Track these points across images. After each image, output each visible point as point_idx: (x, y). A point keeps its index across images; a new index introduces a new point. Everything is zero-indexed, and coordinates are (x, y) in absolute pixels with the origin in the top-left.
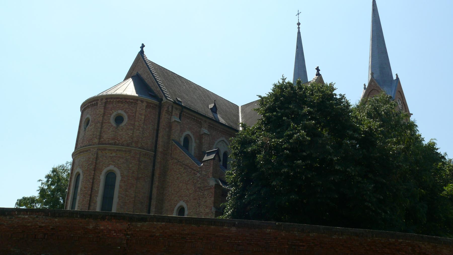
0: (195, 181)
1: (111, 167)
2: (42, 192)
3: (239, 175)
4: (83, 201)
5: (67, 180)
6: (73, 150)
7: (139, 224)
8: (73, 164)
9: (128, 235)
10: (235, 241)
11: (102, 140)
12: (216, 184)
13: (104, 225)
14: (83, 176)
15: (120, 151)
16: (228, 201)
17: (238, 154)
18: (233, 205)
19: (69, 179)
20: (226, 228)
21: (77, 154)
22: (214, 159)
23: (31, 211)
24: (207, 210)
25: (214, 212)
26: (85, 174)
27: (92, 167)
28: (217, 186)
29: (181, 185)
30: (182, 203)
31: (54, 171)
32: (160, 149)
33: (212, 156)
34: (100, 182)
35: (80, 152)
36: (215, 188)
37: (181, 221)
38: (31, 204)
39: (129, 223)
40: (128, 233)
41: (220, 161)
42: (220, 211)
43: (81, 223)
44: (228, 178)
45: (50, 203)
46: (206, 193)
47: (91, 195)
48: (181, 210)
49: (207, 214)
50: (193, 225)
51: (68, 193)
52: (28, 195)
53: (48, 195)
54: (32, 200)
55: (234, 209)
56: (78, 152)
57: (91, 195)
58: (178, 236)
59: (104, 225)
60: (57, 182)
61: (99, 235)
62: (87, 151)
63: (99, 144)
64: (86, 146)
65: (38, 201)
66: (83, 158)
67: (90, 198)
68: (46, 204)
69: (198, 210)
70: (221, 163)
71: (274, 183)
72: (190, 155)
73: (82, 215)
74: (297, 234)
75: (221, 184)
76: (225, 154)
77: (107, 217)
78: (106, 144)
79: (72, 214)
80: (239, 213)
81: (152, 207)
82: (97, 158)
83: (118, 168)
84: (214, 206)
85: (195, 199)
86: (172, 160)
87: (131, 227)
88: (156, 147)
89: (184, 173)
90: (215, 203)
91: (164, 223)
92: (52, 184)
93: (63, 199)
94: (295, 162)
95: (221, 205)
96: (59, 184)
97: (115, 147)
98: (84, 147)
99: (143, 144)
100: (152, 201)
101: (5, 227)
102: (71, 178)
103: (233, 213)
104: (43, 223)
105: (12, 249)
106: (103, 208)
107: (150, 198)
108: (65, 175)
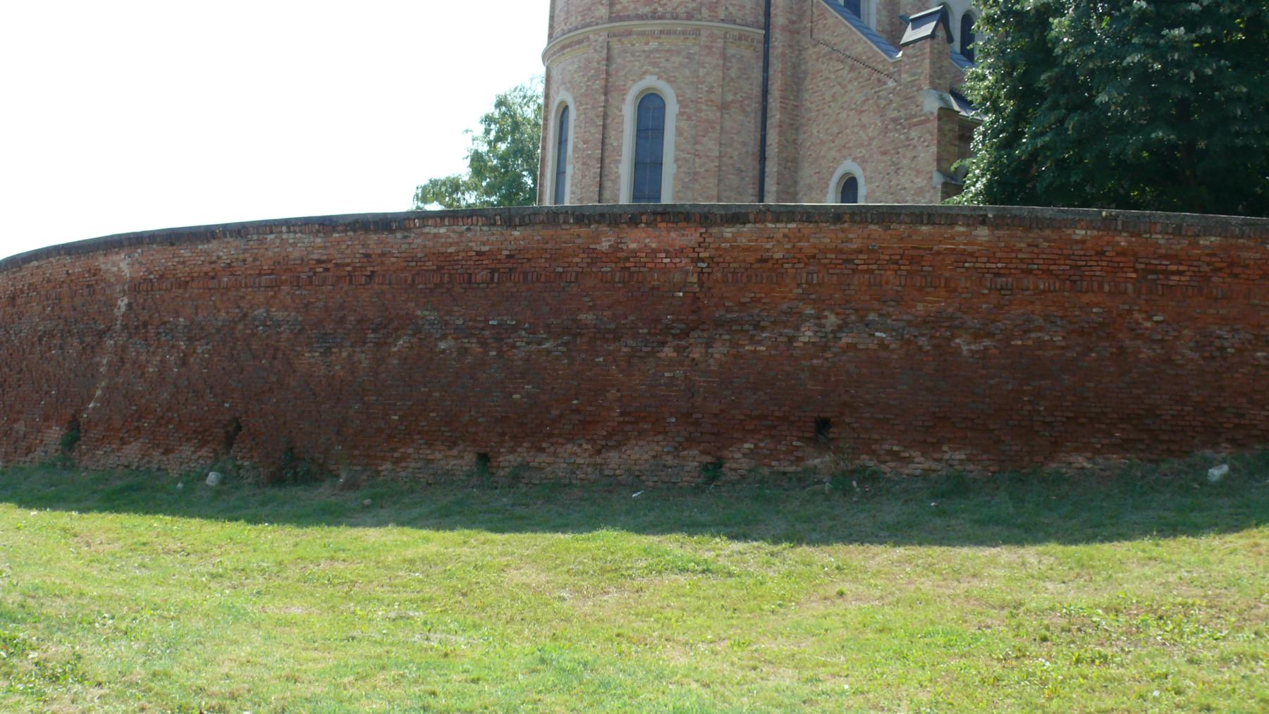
0: (883, 102)
1: (650, 81)
2: (477, 161)
3: (1003, 80)
4: (584, 176)
5: (536, 124)
6: (543, 42)
7: (728, 232)
8: (548, 80)
9: (702, 260)
10: (988, 265)
11: (618, 7)
12: (941, 109)
13: (637, 240)
14: (578, 110)
15: (669, 33)
16: (973, 154)
17: (999, 20)
18: (990, 164)
19: (541, 122)
20: (962, 229)
21: (555, 53)
22: (932, 36)
23: (453, 216)
24: (921, 182)
25: (939, 187)
26: (581, 104)
27: (598, 85)
28: (946, 112)
29: (843, 115)
30: (850, 166)
31: (500, 103)
32: (779, 19)
33: (927, 29)
34: (622, 123)
35: (563, 48)
36: (939, 118)
37: (850, 215)
38: (450, 195)
39: (703, 230)
40: (702, 255)
41: (950, 39)
42: (953, 184)
43: (579, 236)
44: (972, 88)
45: (500, 189)
46: (914, 134)
47: (602, 160)
48: (849, 187)
49: (920, 192)
50: (872, 227)
51: (543, 160)
52: (441, 175)
53: (494, 169)
54: (455, 186)
55: (994, 174)
56: (558, 47)
57: (602, 160)
58: (833, 256)
59: (637, 240)
60: (513, 132)
61: (628, 265)
62: (580, 42)
63: (611, 19)
64: (576, 29)
65: (468, 188)
66: (573, 62)
67: (601, 168)
68: (489, 191)
69: (894, 182)
70: (957, 46)
71: (1102, 98)
72: (865, 30)
73: (581, 217)
74: (1161, 242)
75: (956, 108)
76: (967, 20)
77: (644, 218)
78: (629, 18)
79: (555, 217)
80: (1011, 185)
81: (767, 180)
82: (609, 59)
83: (668, 81)
84: (939, 170)
85: (884, 153)
86: (815, 46)
87: (708, 240)
88: (767, 14)
89: (850, 81)
90: (939, 160)
91: (793, 225)
92: (499, 139)
93: (532, 172)
94: (1165, 32)
95: (955, 165)
96: (517, 136)
97: (655, 25)
98: (570, 31)
99: (731, 9)
100: (768, 163)
101: (393, 260)
102: (546, 119)
103: (988, 186)
104: (484, 244)
105: (419, 313)
106: (637, 195)
107: (763, 158)
108: (529, 113)
